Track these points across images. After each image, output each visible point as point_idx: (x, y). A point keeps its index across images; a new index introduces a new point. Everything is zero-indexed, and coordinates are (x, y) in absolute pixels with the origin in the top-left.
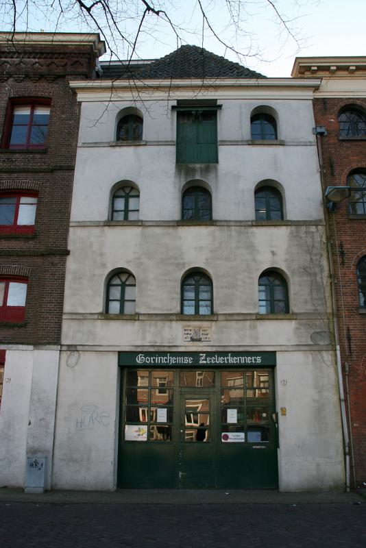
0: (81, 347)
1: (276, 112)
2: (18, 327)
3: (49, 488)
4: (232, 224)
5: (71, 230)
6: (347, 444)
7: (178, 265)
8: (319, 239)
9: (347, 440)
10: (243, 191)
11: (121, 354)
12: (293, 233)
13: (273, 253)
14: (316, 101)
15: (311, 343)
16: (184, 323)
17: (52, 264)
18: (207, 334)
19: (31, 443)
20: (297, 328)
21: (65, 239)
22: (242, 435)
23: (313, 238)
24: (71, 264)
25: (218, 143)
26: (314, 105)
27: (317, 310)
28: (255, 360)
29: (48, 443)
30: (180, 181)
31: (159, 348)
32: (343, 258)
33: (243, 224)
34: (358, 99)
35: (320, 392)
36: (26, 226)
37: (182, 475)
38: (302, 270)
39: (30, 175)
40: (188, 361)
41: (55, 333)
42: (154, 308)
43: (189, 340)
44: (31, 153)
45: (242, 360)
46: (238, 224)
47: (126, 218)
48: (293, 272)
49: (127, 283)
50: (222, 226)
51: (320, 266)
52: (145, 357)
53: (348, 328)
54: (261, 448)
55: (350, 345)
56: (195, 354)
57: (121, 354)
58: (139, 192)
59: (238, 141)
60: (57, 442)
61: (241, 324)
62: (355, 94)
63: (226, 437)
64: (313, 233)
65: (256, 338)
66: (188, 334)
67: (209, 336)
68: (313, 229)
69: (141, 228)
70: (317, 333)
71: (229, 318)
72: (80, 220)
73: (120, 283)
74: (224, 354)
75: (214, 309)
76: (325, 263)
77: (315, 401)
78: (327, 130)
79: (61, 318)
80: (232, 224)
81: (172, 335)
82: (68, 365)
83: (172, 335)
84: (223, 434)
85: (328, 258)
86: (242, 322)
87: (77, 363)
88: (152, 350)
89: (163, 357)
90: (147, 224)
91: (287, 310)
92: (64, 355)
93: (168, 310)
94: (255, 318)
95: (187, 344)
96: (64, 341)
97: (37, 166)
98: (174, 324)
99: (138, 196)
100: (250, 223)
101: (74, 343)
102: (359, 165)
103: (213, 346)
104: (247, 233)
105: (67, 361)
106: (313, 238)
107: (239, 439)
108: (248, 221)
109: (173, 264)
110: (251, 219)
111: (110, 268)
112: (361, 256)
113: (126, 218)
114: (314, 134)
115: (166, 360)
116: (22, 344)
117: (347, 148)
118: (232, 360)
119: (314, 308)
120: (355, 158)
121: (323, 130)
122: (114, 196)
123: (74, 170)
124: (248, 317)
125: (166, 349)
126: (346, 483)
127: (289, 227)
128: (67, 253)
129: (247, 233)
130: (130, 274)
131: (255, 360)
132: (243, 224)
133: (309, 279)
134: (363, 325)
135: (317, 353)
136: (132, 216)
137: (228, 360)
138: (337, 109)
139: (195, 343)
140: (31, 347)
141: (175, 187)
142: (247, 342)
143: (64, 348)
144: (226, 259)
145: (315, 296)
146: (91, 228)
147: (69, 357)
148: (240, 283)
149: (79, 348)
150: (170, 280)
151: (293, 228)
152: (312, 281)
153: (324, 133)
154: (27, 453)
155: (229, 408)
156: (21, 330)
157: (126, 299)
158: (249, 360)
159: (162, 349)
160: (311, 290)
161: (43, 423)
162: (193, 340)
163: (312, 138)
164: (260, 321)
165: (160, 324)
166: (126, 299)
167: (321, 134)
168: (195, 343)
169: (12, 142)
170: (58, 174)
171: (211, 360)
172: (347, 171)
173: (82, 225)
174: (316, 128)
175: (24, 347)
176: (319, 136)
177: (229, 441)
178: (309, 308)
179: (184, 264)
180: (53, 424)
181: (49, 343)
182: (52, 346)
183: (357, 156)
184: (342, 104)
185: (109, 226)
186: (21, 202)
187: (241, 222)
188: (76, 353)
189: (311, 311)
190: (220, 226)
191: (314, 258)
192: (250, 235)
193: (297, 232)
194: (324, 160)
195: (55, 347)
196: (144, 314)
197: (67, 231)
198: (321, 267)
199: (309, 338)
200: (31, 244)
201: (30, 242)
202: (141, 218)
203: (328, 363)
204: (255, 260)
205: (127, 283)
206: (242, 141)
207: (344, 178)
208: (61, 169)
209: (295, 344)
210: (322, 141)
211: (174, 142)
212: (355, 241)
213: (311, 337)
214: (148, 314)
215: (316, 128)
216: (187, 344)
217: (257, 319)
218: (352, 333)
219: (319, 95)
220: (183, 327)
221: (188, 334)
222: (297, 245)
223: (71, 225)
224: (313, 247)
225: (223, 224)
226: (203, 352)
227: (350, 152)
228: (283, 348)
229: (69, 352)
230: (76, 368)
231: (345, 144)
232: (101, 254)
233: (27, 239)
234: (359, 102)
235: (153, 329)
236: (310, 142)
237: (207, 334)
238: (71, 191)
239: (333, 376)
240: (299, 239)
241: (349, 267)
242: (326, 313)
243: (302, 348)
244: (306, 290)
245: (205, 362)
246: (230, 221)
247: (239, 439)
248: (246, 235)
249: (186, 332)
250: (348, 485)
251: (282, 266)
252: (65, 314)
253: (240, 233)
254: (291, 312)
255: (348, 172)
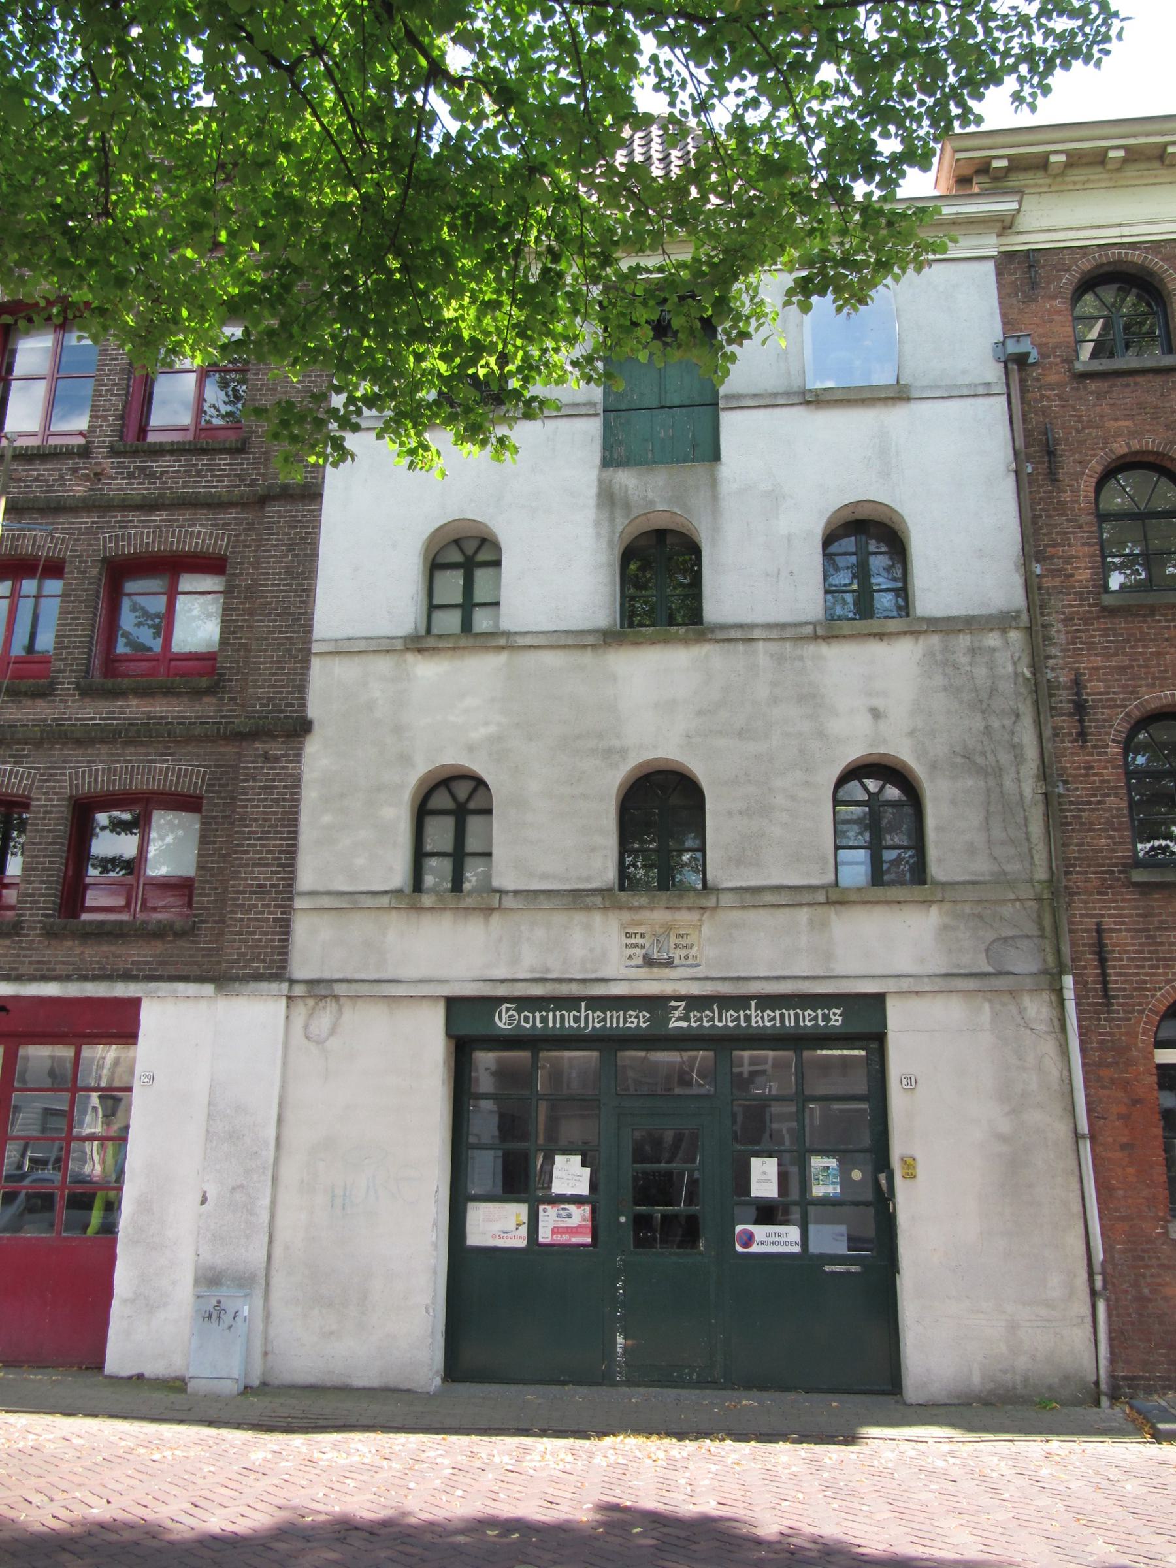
0: (344, 986)
1: (829, 523)
2: (176, 934)
3: (256, 1383)
4: (757, 634)
5: (316, 663)
6: (1097, 1267)
7: (609, 752)
8: (1010, 669)
9: (1099, 1255)
10: (789, 538)
11: (453, 1005)
12: (933, 654)
13: (876, 714)
14: (1006, 262)
15: (990, 969)
16: (626, 916)
17: (266, 758)
18: (689, 947)
19: (207, 1256)
20: (946, 927)
21: (301, 690)
22: (793, 1232)
23: (991, 665)
24: (312, 747)
25: (722, 404)
26: (999, 273)
27: (1005, 873)
28: (826, 1018)
29: (255, 1255)
30: (612, 520)
31: (557, 985)
32: (1081, 721)
33: (788, 633)
34: (1133, 246)
35: (1014, 1112)
36: (196, 653)
37: (625, 1348)
38: (959, 760)
39: (203, 516)
40: (637, 1021)
41: (272, 947)
42: (544, 876)
43: (640, 961)
44: (204, 451)
45: (790, 1019)
46: (775, 634)
47: (467, 626)
48: (934, 766)
49: (472, 805)
50: (729, 640)
51: (1014, 747)
52: (519, 1010)
53: (1099, 924)
54: (848, 1273)
55: (1104, 975)
56: (656, 1004)
57: (453, 1005)
58: (500, 549)
59: (775, 395)
60: (278, 1252)
61: (783, 916)
62: (1126, 231)
63: (749, 1239)
64: (994, 650)
65: (829, 956)
66: (636, 946)
67: (694, 951)
68: (992, 640)
69: (503, 657)
70: (1005, 940)
71: (749, 899)
72: (339, 635)
73: (449, 804)
74: (739, 1002)
75: (709, 877)
76: (1027, 737)
77: (1003, 1138)
78: (1039, 346)
79: (291, 906)
80: (757, 634)
81: (591, 950)
82: (307, 1037)
83: (591, 950)
84: (739, 1228)
85: (1038, 723)
86: (787, 910)
87: (333, 1031)
88: (538, 991)
89: (569, 1011)
90: (522, 641)
91: (919, 873)
92: (300, 1012)
93: (579, 879)
94: (822, 899)
95: (633, 973)
96: (301, 968)
97: (221, 489)
98: (597, 918)
99: (497, 563)
100: (809, 630)
101: (327, 975)
102: (1136, 445)
103: (707, 979)
104: (801, 658)
105: (306, 1027)
106: (991, 665)
107: (785, 1244)
108: (806, 623)
109: (593, 751)
110: (810, 618)
111: (420, 768)
112: (1137, 714)
113: (467, 626)
114: (999, 360)
115: (577, 1019)
116: (185, 979)
117: (1099, 396)
118: (761, 1020)
119: (996, 868)
120: (1122, 423)
121: (1025, 346)
122: (435, 566)
123: (321, 495)
124: (807, 897)
125: (575, 990)
126: (1097, 1383)
127: (922, 638)
128: (303, 727)
129: (801, 658)
130: (479, 783)
131: (826, 1018)
132: (788, 633)
133: (982, 783)
134: (1145, 916)
135: (1006, 998)
136: (482, 621)
137: (748, 1018)
138: (1068, 280)
139: (657, 972)
140: (208, 989)
141: (598, 535)
142: (802, 967)
143: (299, 990)
144: (741, 734)
145: (998, 833)
146: (371, 657)
147: (311, 1015)
148: (780, 800)
149: (339, 989)
150: (585, 797)
151: (935, 640)
152: (988, 790)
153: (1027, 355)
154: (197, 1282)
155: (758, 1154)
156: (181, 943)
157: (477, 600)
158: (807, 1019)
159: (564, 990)
160: (987, 819)
161: (238, 1196)
162: (649, 962)
163: (993, 373)
164: (838, 907)
165: (559, 918)
166: (477, 600)
167: (1021, 360)
168: (655, 970)
169: (155, 421)
170: (275, 510)
171: (700, 1019)
172: (1096, 466)
173: (346, 650)
174: (1003, 343)
175: (191, 988)
176: (1013, 367)
177: (755, 1249)
178: (981, 867)
179: (623, 752)
180: (266, 1202)
181: (258, 978)
182: (264, 986)
183: (1128, 417)
184: (1086, 265)
185: (420, 651)
186: (180, 589)
187: (782, 626)
188: (331, 1006)
189: (987, 878)
190: (724, 641)
191: (996, 724)
192: (809, 663)
193: (945, 649)
194: (1028, 434)
195: (274, 986)
196: (516, 893)
197: (306, 666)
198: (1017, 750)
199: (983, 955)
200: (208, 707)
201: (206, 700)
202: (506, 624)
203: (1042, 1027)
204: (821, 734)
205: (472, 805)
206: (787, 394)
207: (1086, 486)
208: (286, 494)
209: (943, 971)
210: (1022, 381)
211: (595, 405)
212: (1122, 669)
213: (987, 950)
214: (528, 891)
215: (1003, 343)
216: (633, 973)
217: (829, 903)
218: (1110, 940)
219: (1017, 243)
220: (623, 926)
221: (636, 946)
222: (945, 689)
223: (316, 648)
224: (993, 691)
225: (733, 634)
226: (679, 998)
227: (1107, 409)
228: (905, 985)
229: (311, 1002)
230: (333, 1043)
231: (1093, 386)
232: (398, 730)
233: (197, 693)
234: (1136, 256)
235: (540, 933)
236: (988, 384)
237: (689, 947)
238: (314, 556)
239: (1053, 1069)
240: (949, 670)
241: (1101, 749)
242: (1031, 881)
243: (961, 984)
244: (975, 818)
245: (684, 1024)
246: (752, 626)
247: (785, 1244)
248: (798, 664)
249: (632, 941)
250: (1104, 1386)
251: (905, 752)
252: (300, 894)
253: (780, 659)
254: (929, 880)
255: (1099, 469)
